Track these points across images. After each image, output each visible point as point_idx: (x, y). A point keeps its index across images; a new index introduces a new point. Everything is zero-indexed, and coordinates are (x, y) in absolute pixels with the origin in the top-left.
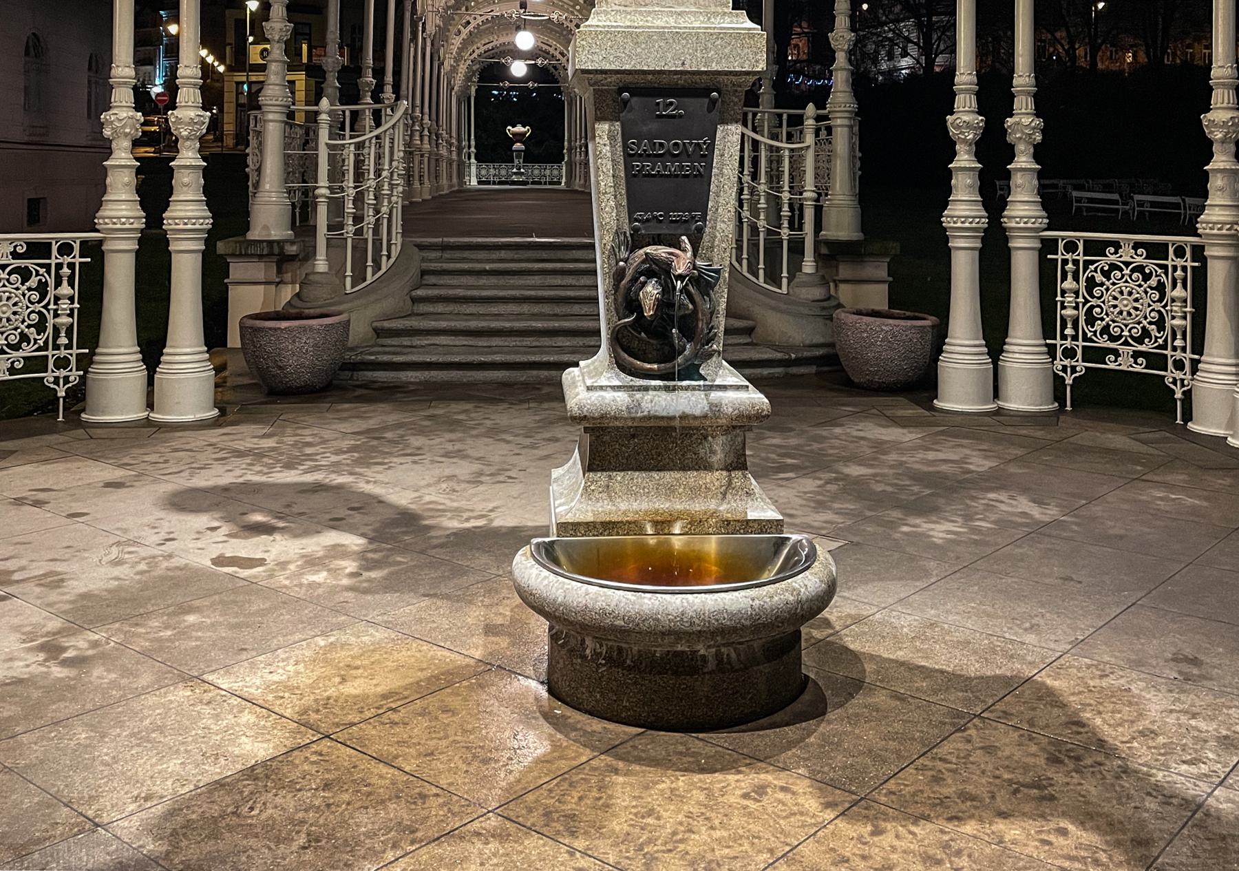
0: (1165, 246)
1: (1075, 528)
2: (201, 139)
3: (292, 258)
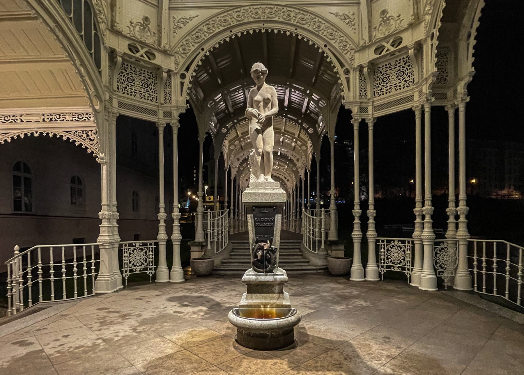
0: (405, 241)
3: (205, 246)
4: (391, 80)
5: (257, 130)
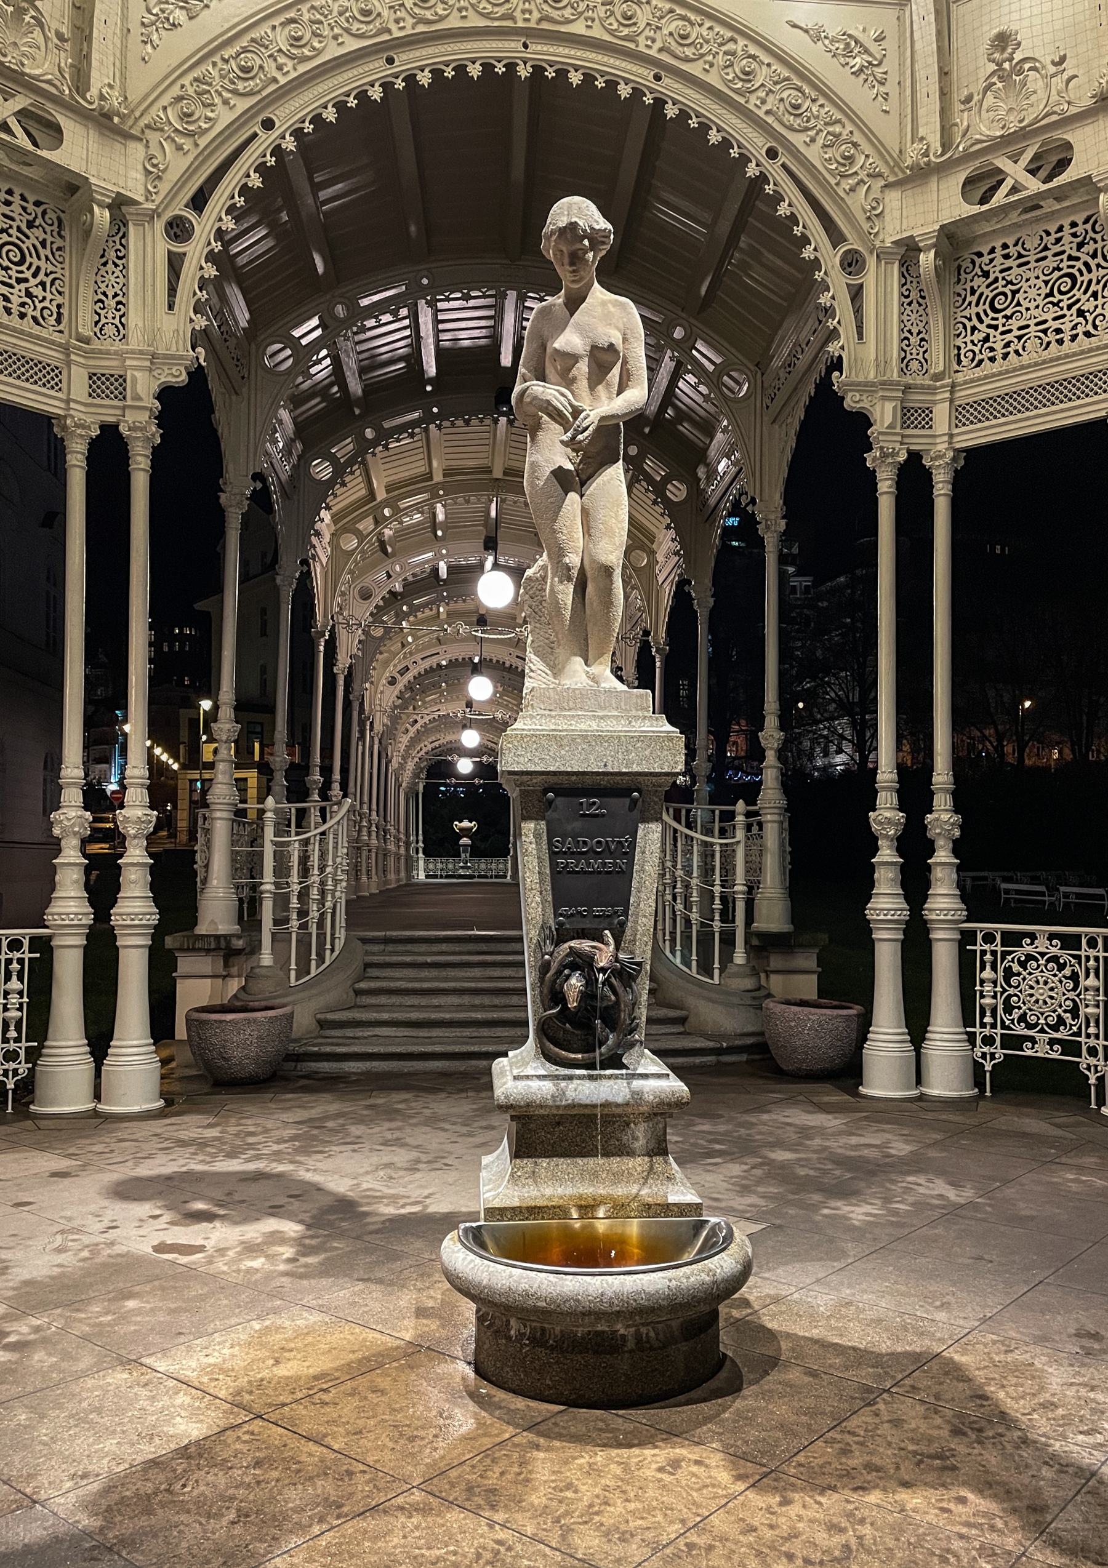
0: (1078, 937)
1: (989, 1209)
2: (148, 838)
3: (239, 952)
4: (1025, 304)
5: (559, 474)
